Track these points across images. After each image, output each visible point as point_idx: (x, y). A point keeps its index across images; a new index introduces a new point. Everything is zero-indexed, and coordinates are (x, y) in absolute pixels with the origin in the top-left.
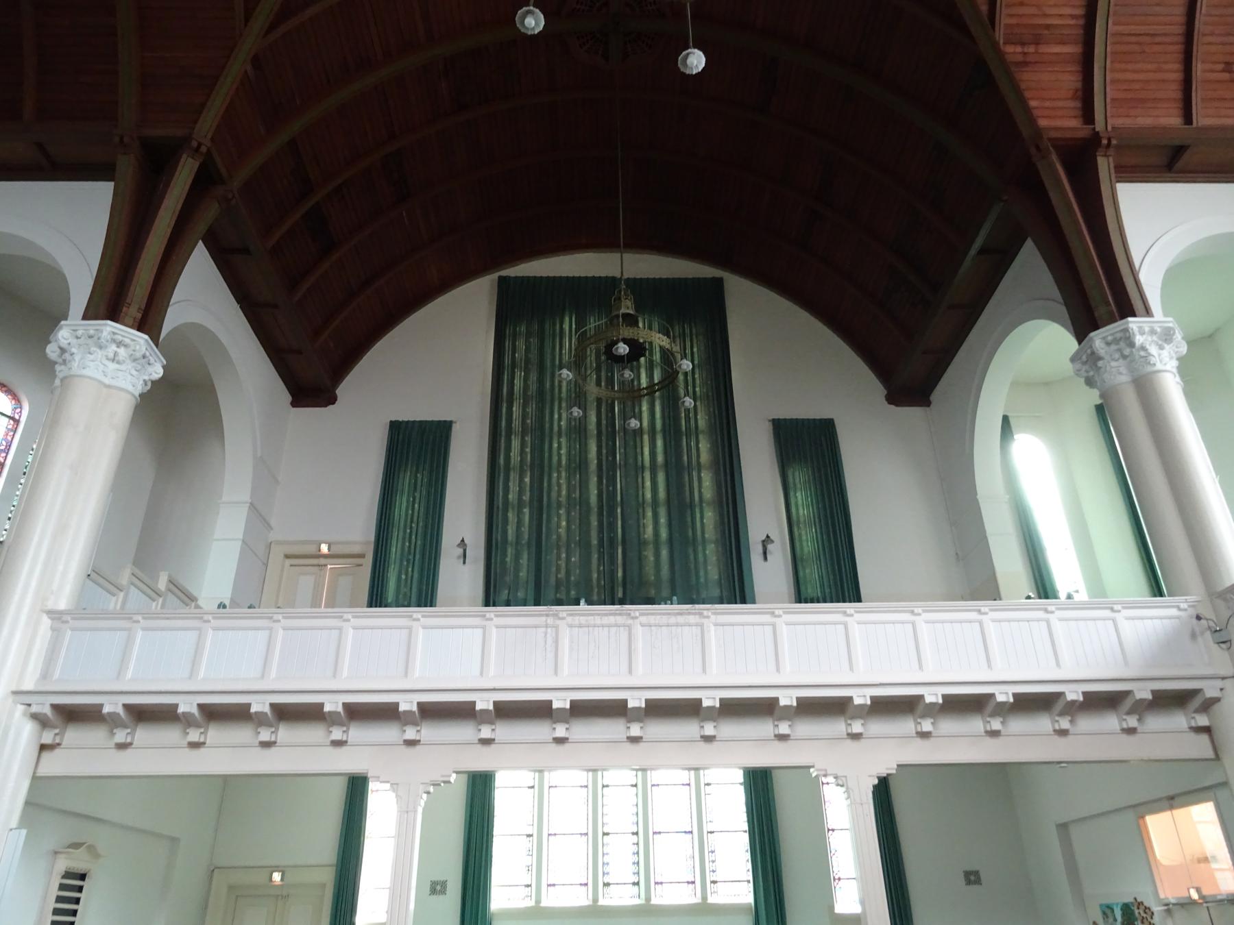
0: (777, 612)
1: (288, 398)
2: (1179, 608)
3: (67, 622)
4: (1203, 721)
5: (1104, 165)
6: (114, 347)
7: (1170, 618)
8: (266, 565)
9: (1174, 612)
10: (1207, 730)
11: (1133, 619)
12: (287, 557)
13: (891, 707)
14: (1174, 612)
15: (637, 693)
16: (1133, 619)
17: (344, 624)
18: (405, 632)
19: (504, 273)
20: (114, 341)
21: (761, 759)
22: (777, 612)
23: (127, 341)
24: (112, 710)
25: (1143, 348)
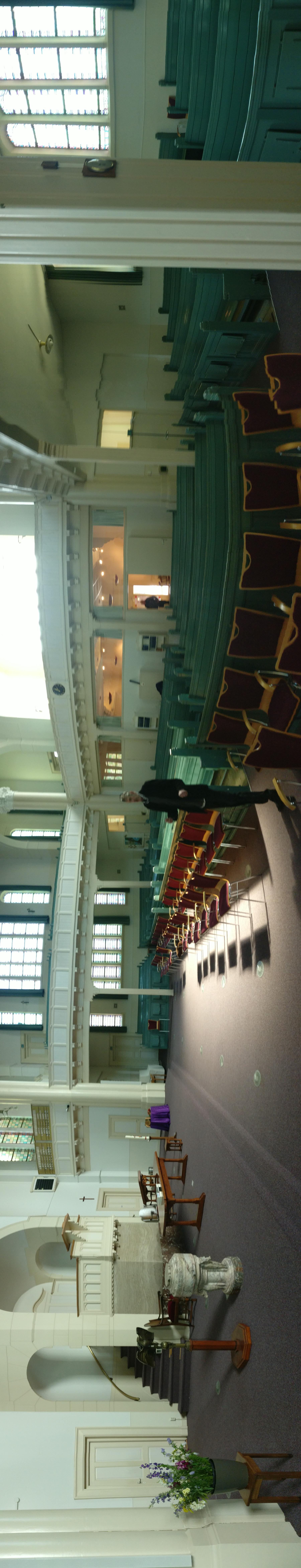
13: (83, 872)
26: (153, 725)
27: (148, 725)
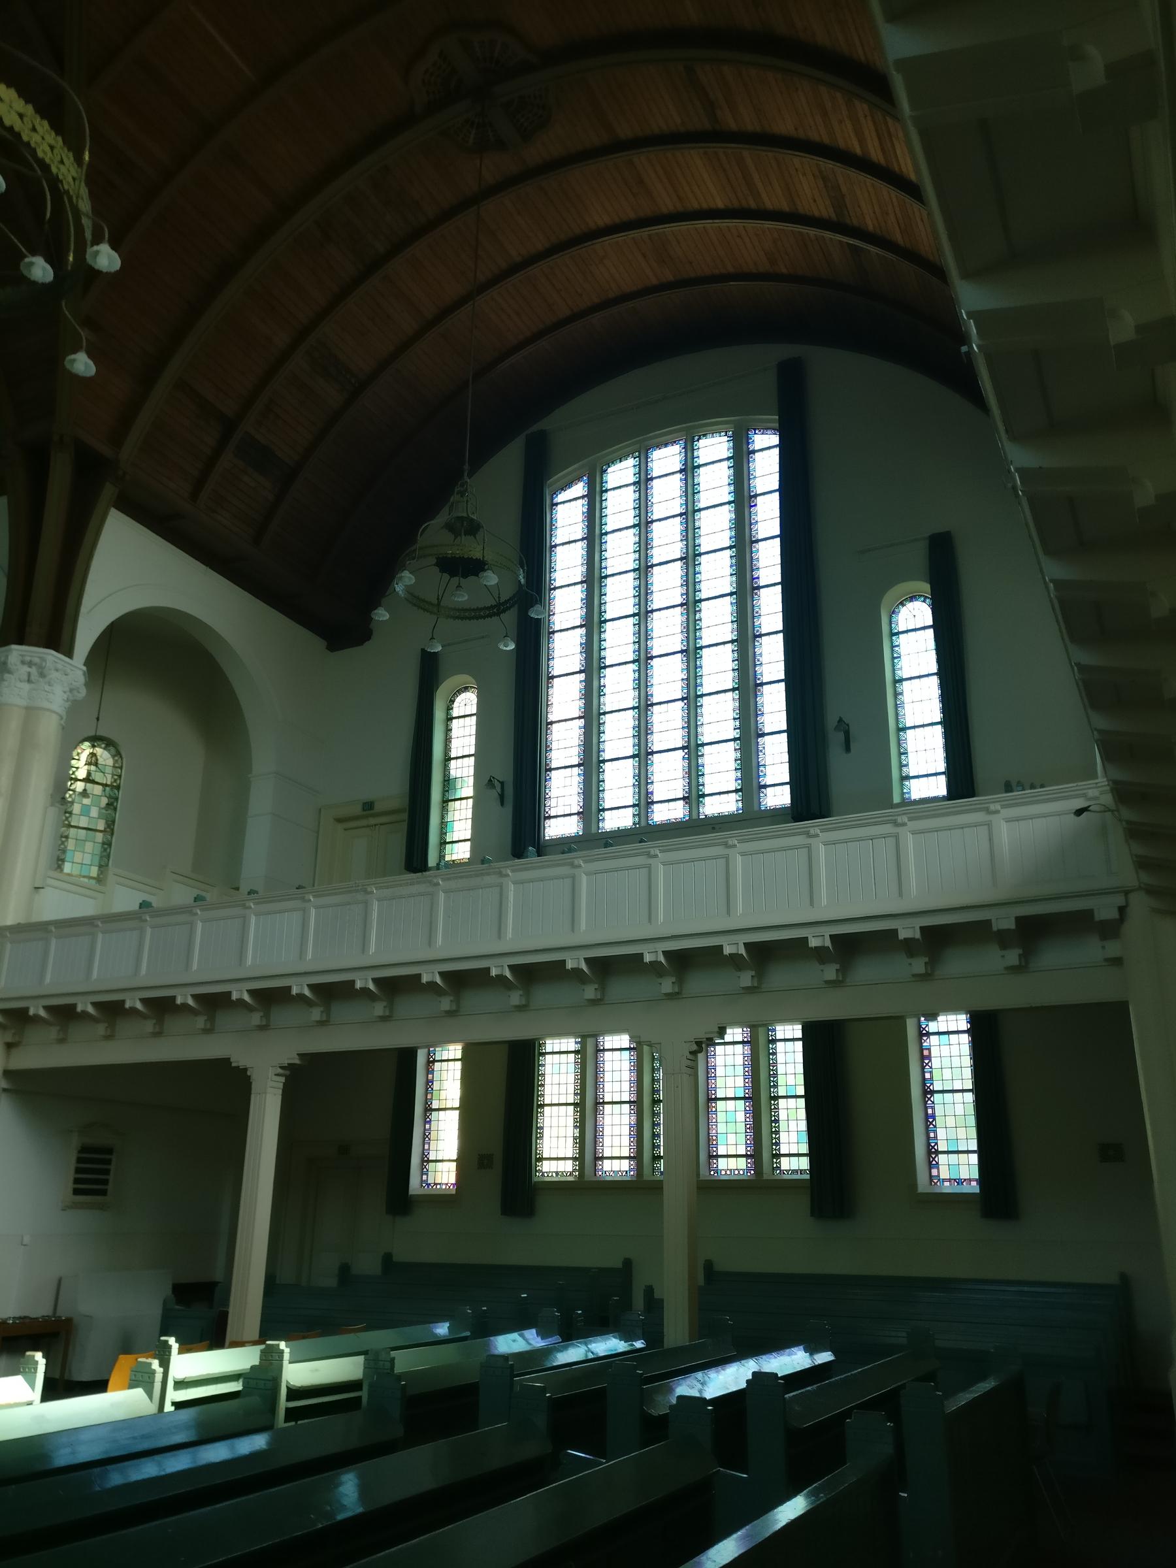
0: (992, 807)
1: (319, 644)
2: (1084, 796)
3: (735, 846)
5: (109, 490)
6: (26, 669)
7: (1059, 814)
8: (318, 832)
10: (1117, 962)
11: (1018, 819)
12: (339, 820)
15: (651, 946)
16: (1018, 819)
17: (651, 861)
18: (568, 881)
19: (529, 431)
20: (23, 663)
21: (829, 1009)
22: (812, 831)
23: (36, 660)
24: (575, 966)
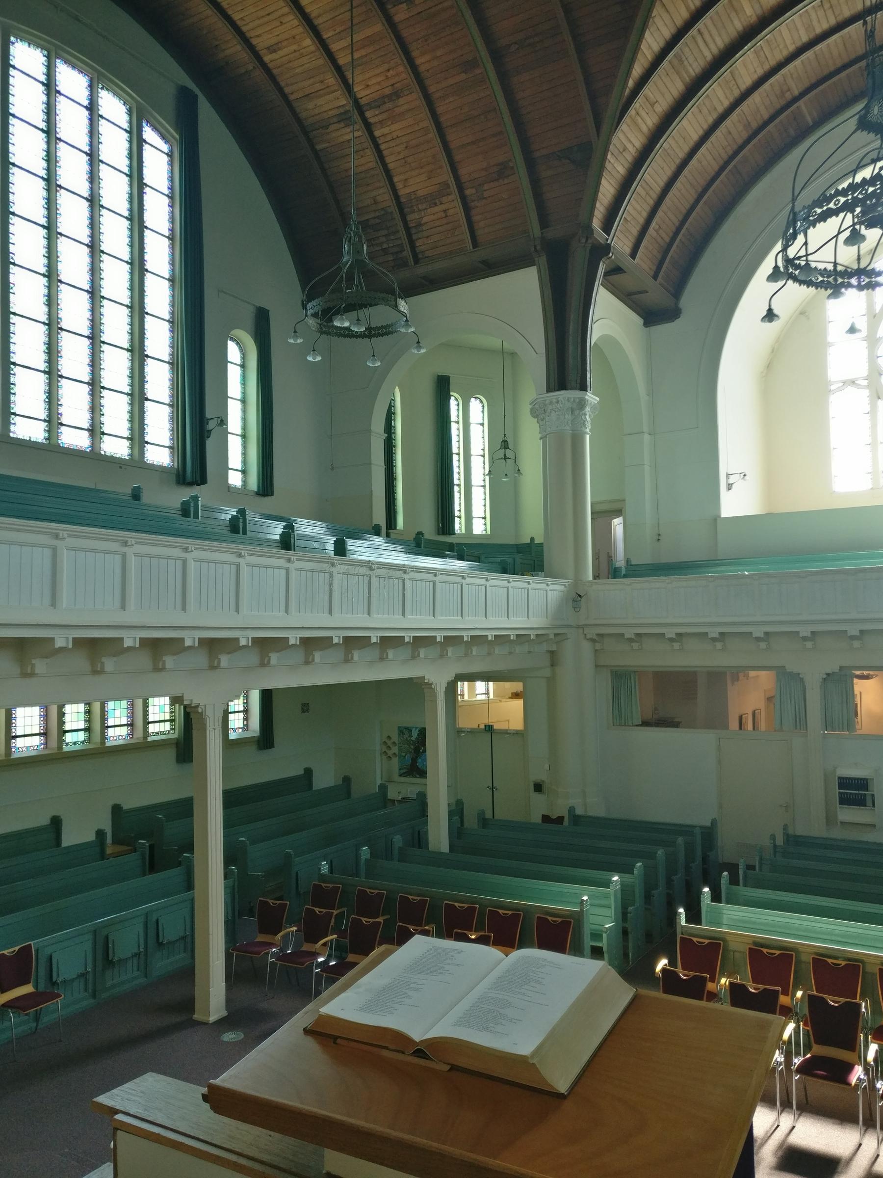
4: (554, 648)
9: (562, 588)
10: (552, 653)
14: (562, 588)
25: (585, 415)
26: (849, 814)
27: (845, 801)
